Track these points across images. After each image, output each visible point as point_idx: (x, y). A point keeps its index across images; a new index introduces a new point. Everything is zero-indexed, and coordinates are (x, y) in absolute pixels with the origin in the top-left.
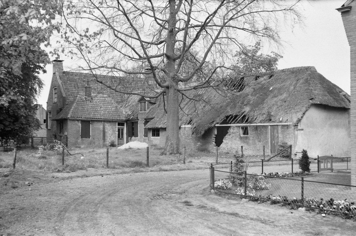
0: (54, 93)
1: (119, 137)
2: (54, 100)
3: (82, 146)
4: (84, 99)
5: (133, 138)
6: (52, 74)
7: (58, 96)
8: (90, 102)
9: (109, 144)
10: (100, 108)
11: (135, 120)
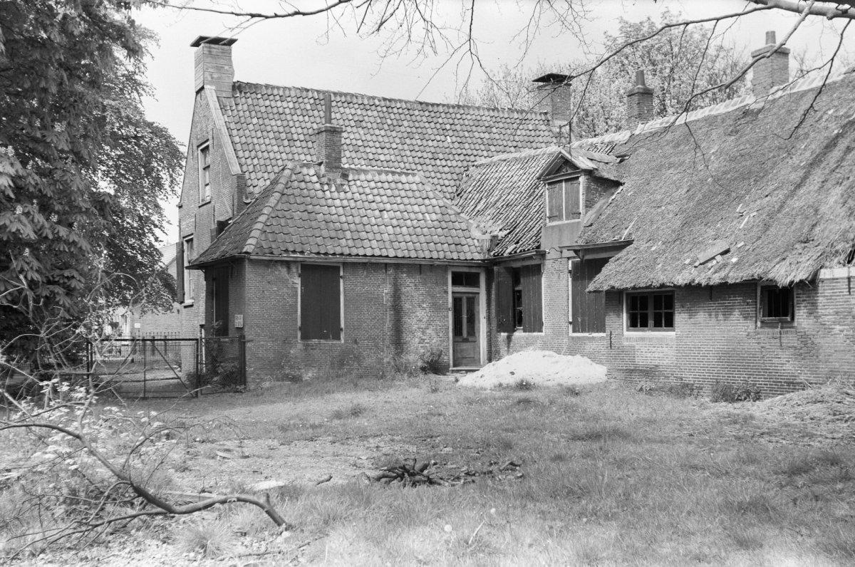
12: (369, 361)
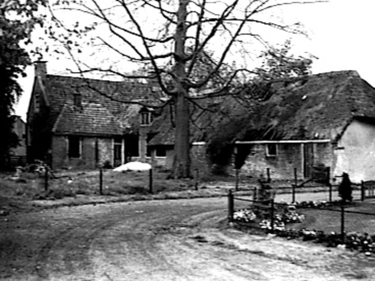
9: (103, 165)
12: (87, 164)
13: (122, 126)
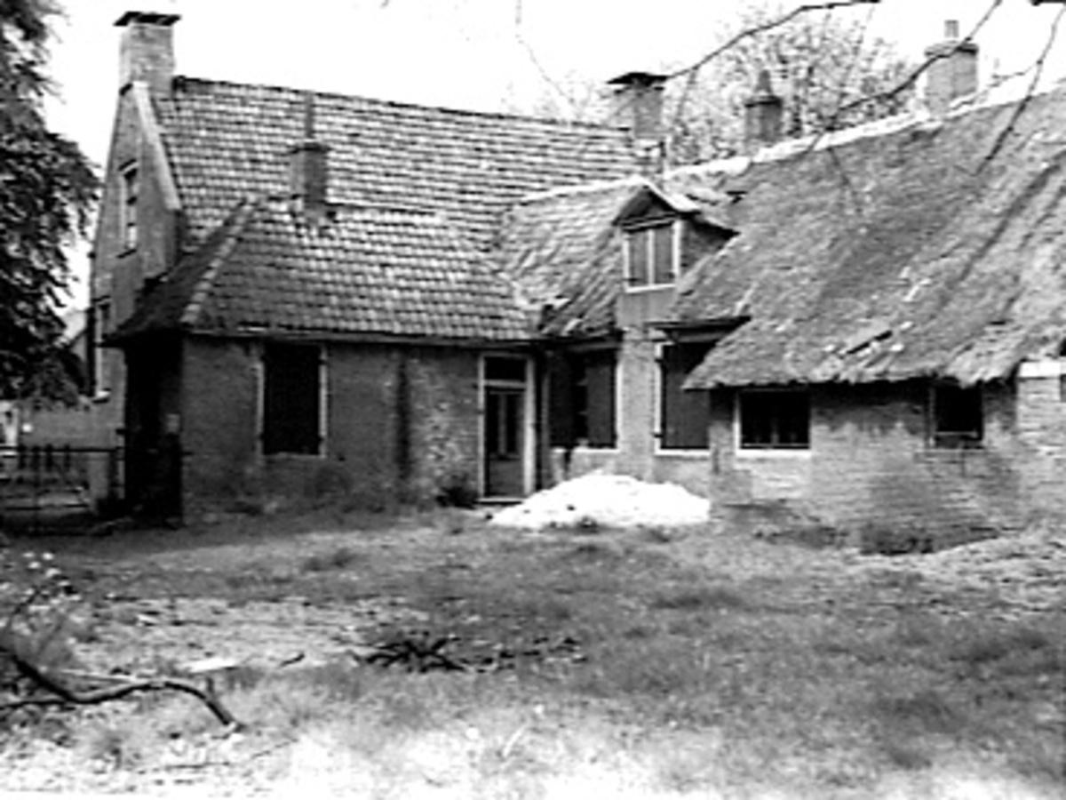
0: (124, 197)
1: (491, 444)
2: (122, 236)
3: (271, 506)
4: (287, 218)
5: (582, 452)
6: (115, 94)
7: (142, 215)
8: (321, 236)
9: (436, 491)
10: (377, 269)
11: (600, 339)
12: (359, 487)
13: (522, 302)
